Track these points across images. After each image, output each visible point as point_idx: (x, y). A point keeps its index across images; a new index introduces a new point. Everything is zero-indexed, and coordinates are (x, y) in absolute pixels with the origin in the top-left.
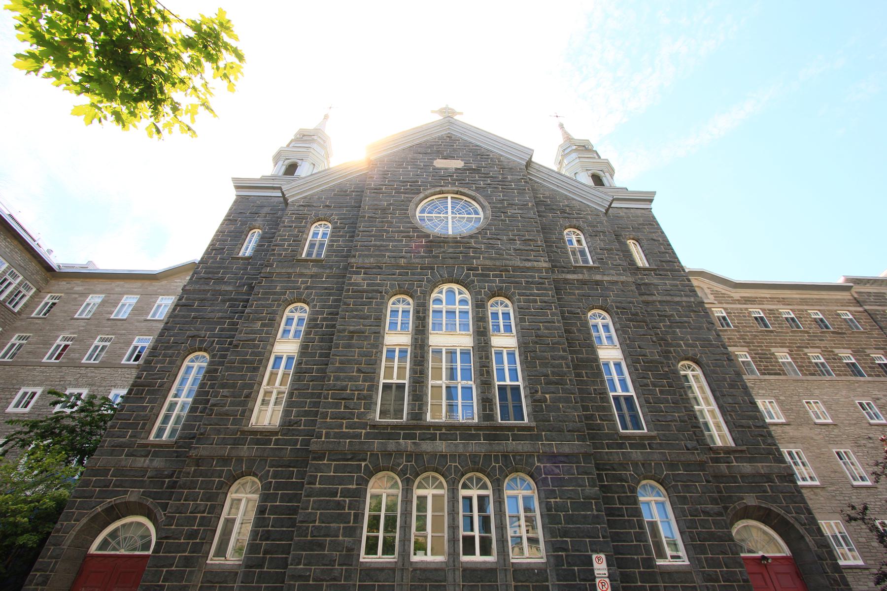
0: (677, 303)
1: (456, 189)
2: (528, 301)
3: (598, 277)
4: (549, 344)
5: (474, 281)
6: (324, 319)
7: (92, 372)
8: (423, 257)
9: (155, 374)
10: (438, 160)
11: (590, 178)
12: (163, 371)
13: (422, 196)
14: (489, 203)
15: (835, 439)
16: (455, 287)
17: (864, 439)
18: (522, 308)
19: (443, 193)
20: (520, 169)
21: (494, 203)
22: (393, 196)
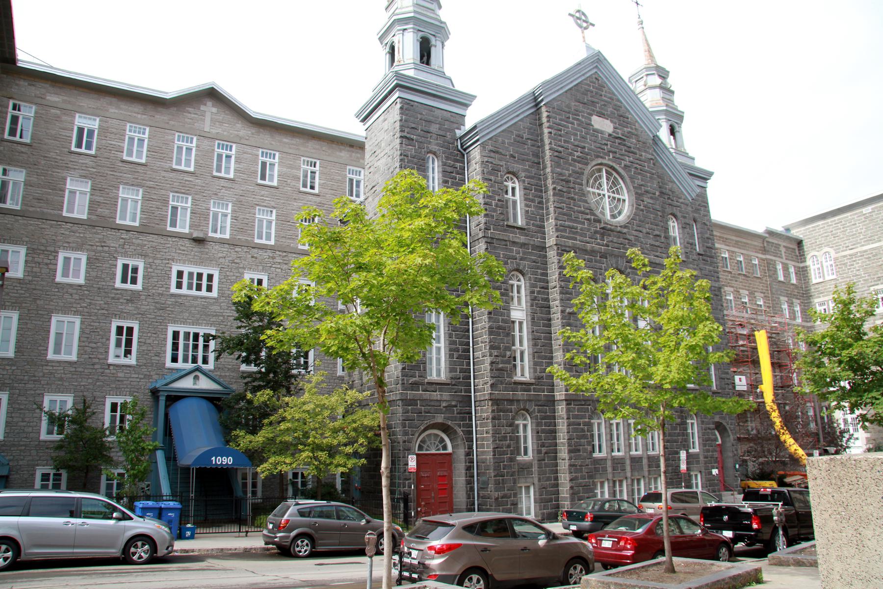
1: (611, 163)
6: (539, 292)
7: (137, 238)
11: (419, 44)
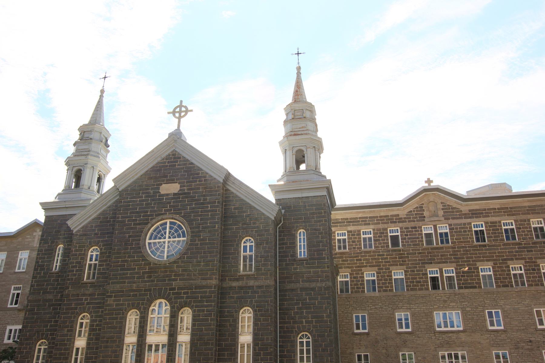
0: (313, 289)
2: (199, 311)
3: (251, 283)
4: (205, 341)
5: (172, 299)
6: (97, 325)
8: (146, 282)
9: (24, 356)
10: (163, 185)
12: (27, 354)
13: (149, 225)
14: (191, 228)
15: (498, 343)
16: (163, 301)
17: (524, 342)
18: (195, 317)
19: (163, 220)
20: (218, 187)
21: (193, 228)
22: (132, 228)
